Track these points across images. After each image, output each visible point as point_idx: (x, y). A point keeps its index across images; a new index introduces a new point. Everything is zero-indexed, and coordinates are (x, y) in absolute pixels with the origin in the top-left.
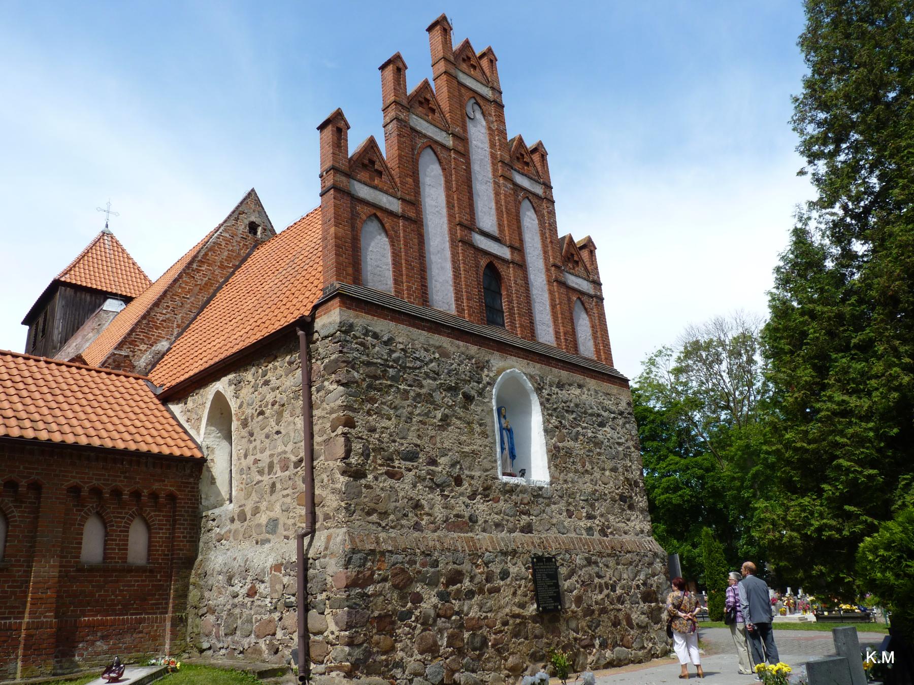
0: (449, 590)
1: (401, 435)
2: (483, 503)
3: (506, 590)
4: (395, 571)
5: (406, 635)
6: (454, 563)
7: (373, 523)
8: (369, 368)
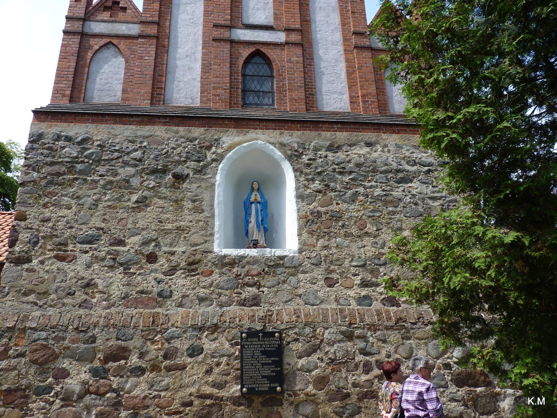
0: (107, 366)
1: (81, 221)
2: (185, 278)
3: (196, 368)
4: (35, 347)
5: (39, 409)
6: (118, 339)
7: (28, 303)
8: (53, 167)
